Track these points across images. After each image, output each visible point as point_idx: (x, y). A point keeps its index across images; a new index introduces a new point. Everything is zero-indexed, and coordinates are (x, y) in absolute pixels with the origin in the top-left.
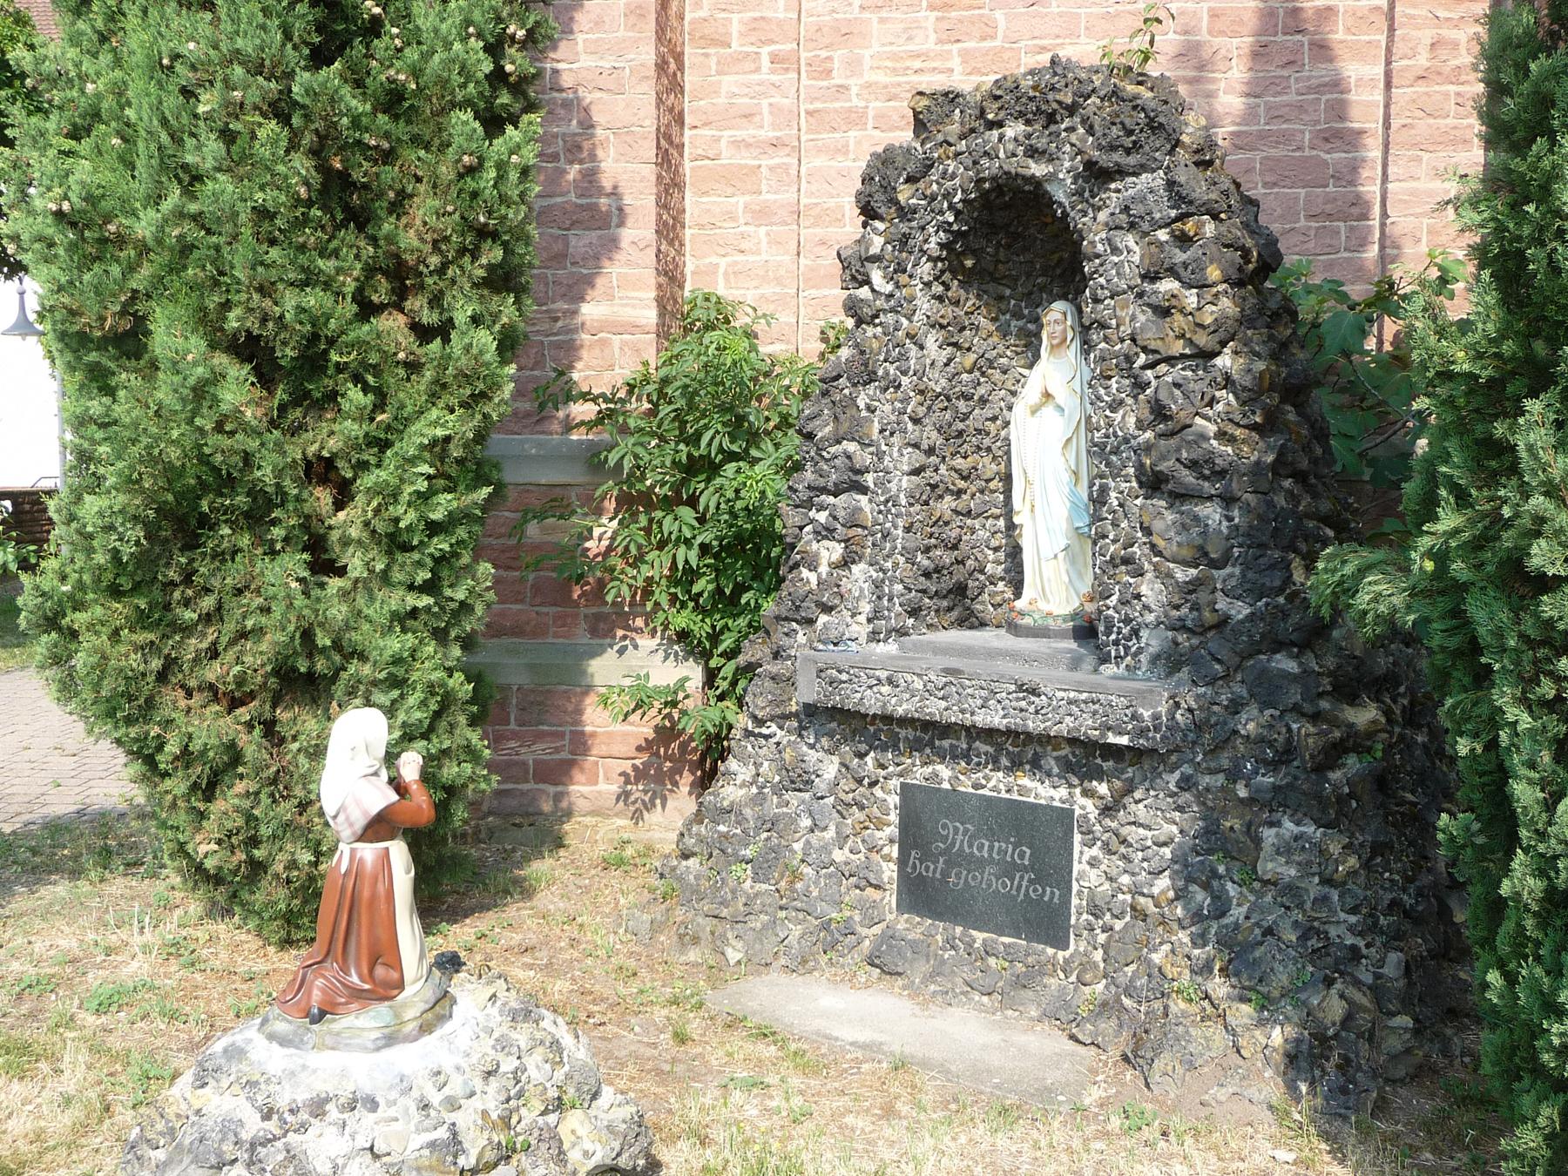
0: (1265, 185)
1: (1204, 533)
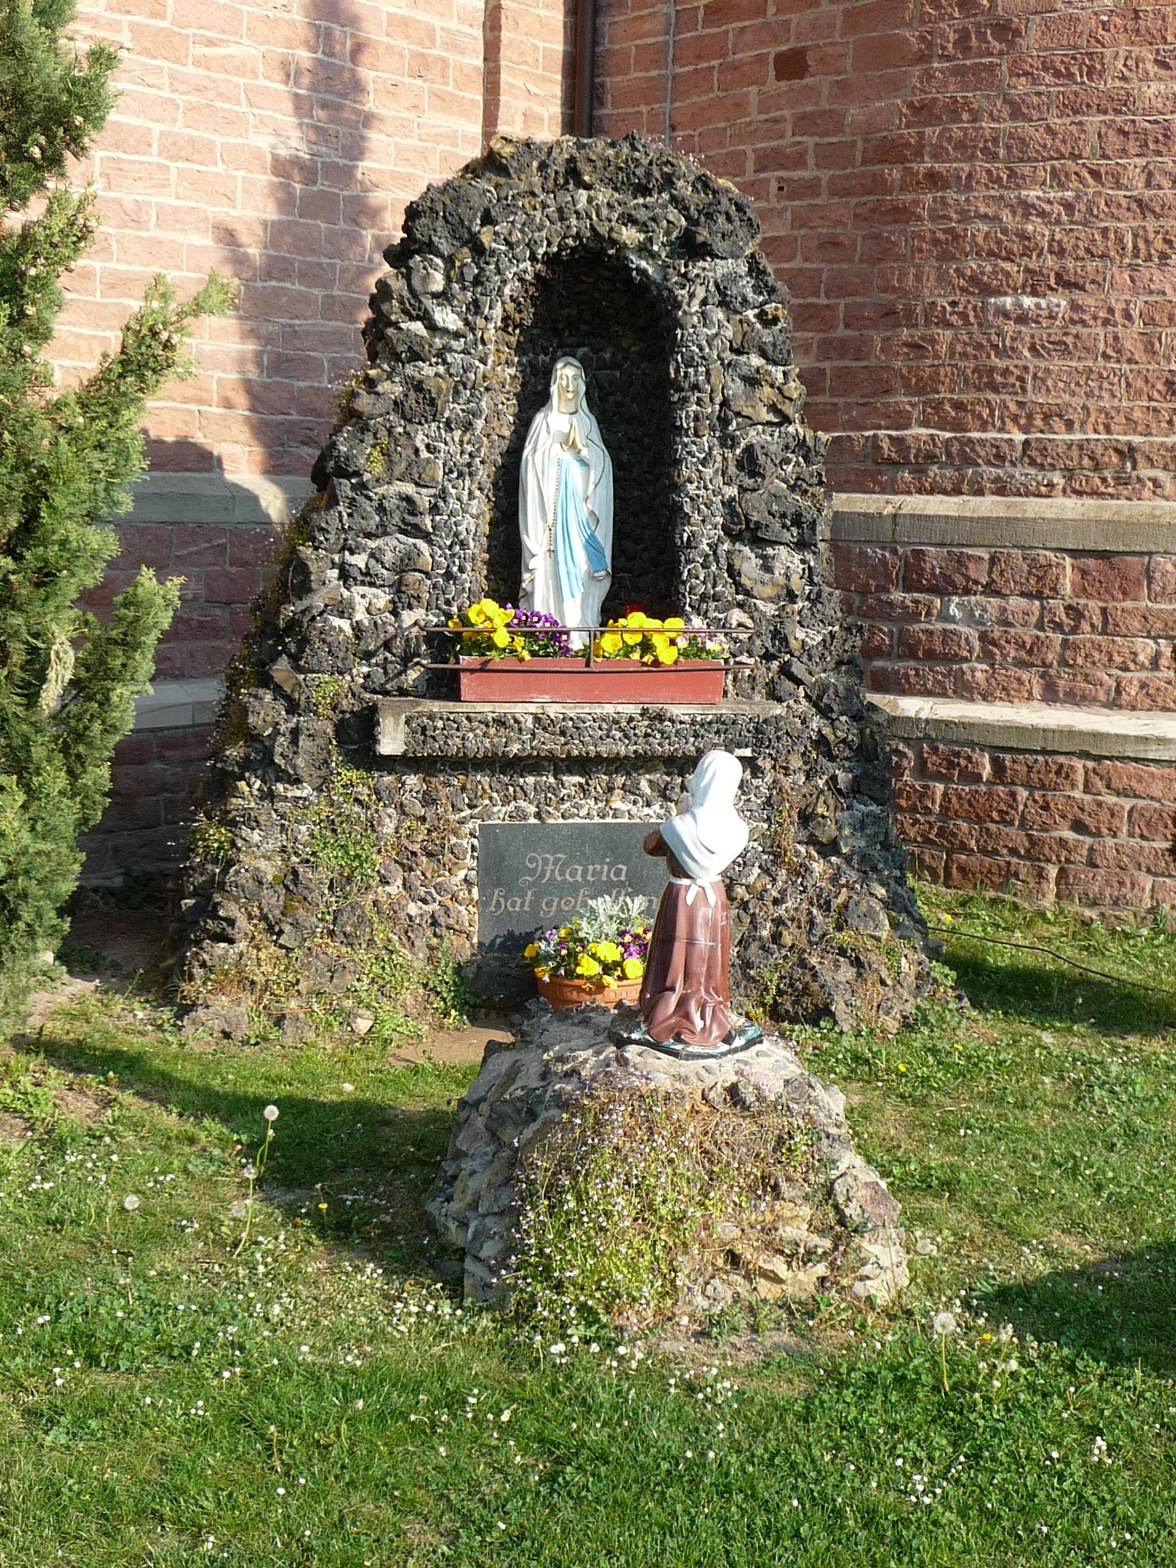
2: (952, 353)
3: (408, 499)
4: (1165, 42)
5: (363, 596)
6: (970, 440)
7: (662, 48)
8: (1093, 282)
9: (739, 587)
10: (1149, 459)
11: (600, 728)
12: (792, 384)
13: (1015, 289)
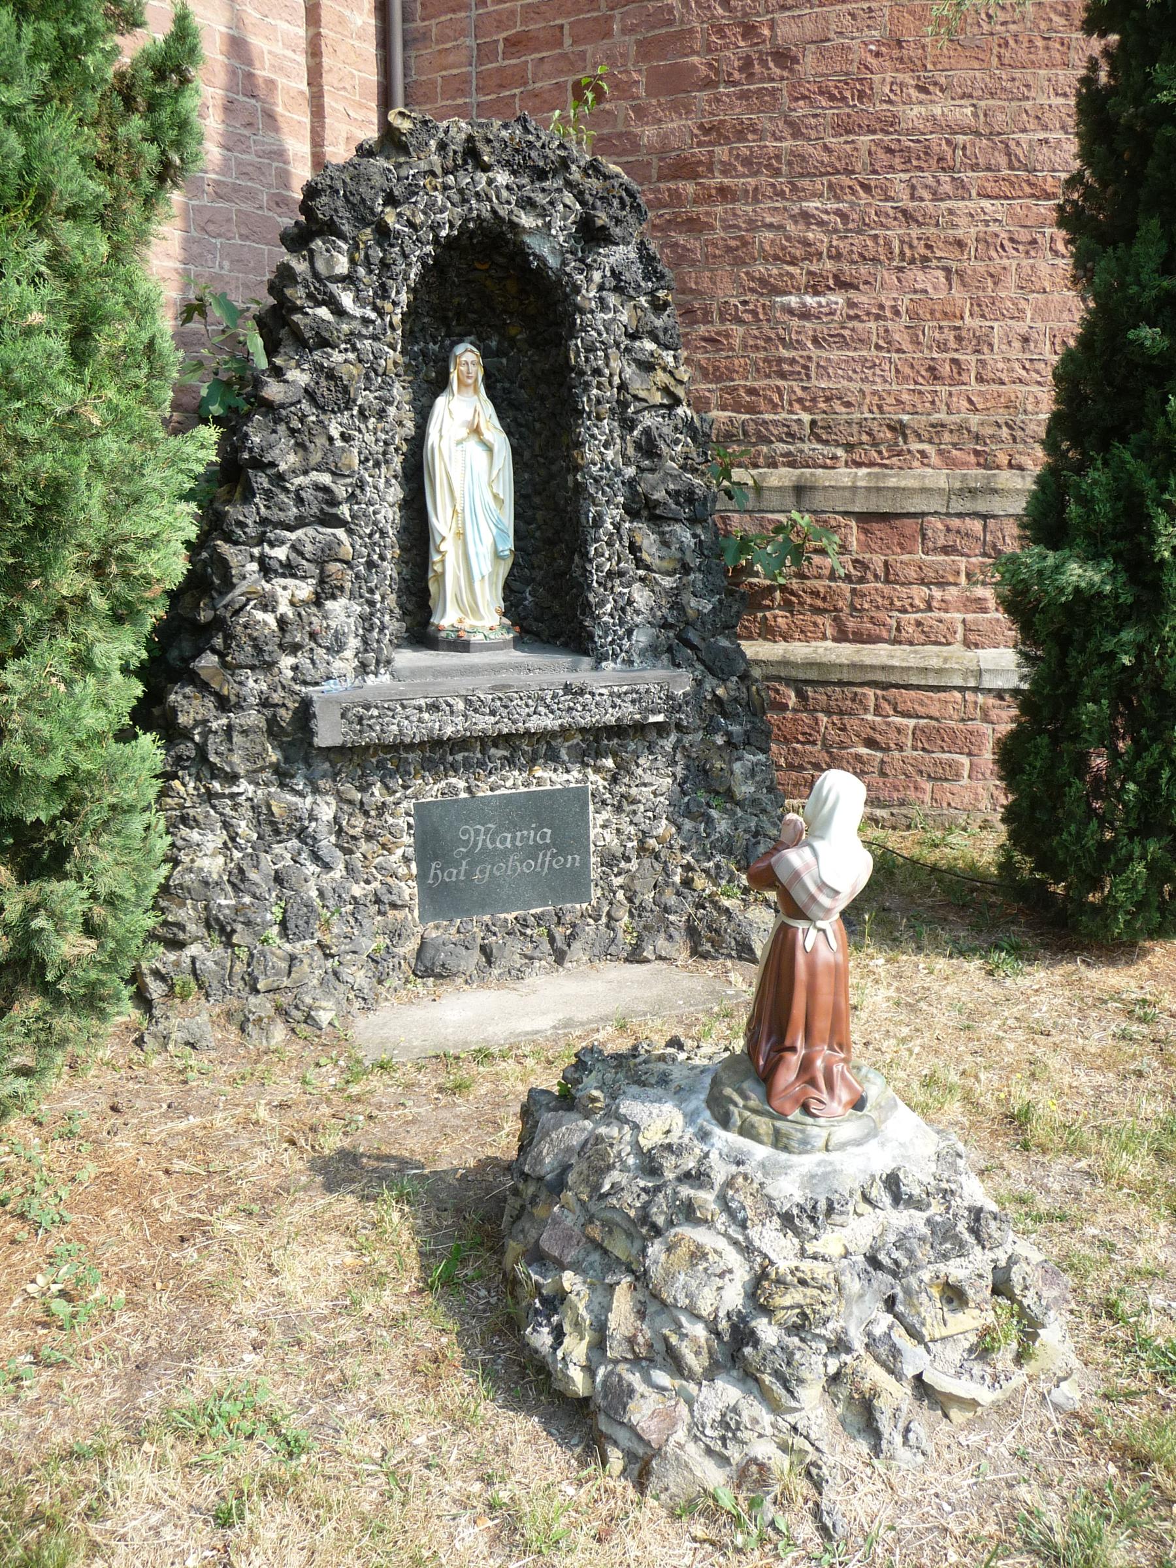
0: (243, 237)
1: (681, 550)
2: (745, 346)
3: (326, 489)
4: (926, 70)
5: (285, 588)
6: (765, 422)
7: (465, 79)
8: (866, 283)
9: (640, 563)
10: (919, 436)
11: (527, 706)
12: (682, 368)
13: (799, 289)
